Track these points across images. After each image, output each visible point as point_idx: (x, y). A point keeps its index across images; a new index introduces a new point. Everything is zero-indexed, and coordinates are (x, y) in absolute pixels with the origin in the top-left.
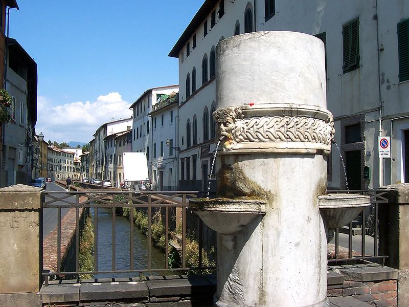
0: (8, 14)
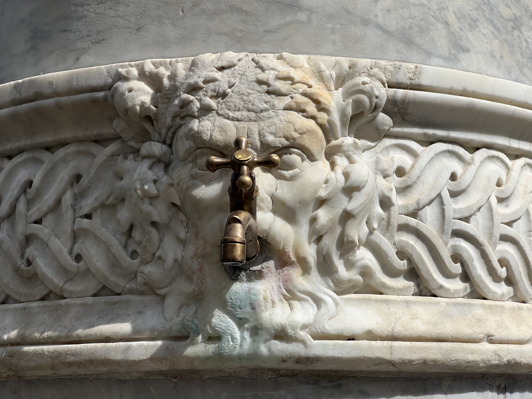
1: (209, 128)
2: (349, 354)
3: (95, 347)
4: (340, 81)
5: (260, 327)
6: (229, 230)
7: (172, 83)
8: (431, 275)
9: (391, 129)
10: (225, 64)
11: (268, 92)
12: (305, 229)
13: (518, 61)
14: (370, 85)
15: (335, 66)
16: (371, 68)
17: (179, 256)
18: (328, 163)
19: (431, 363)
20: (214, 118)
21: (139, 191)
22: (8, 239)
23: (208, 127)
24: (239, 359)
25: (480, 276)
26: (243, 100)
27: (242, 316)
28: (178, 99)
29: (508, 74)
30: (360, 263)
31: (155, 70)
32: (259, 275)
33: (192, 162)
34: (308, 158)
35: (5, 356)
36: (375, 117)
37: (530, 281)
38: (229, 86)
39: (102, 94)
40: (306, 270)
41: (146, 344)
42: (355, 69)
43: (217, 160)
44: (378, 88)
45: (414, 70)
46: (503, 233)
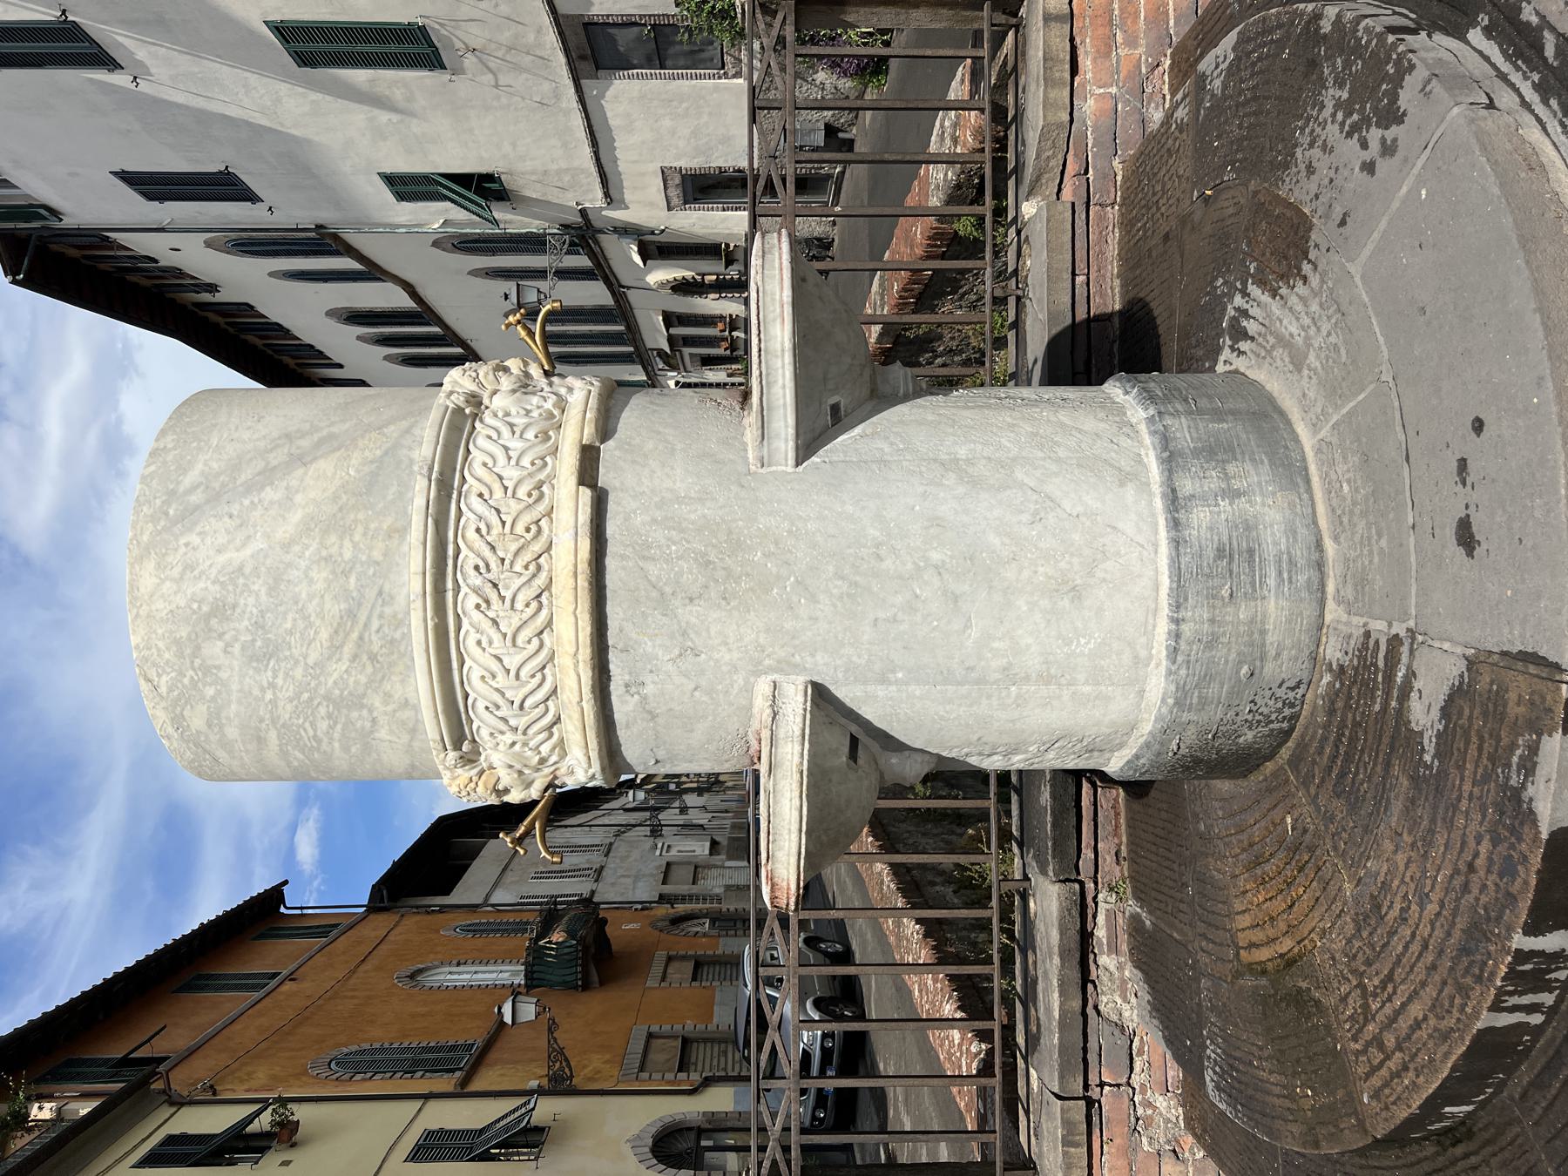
0: (302, 908)
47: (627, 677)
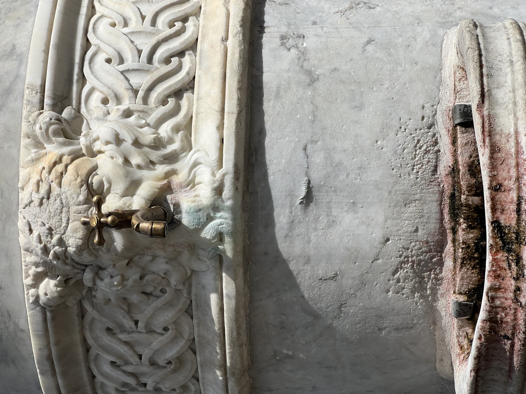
1: (74, 240)
2: (233, 143)
3: (227, 318)
4: (39, 145)
5: (213, 206)
6: (144, 232)
7: (41, 265)
8: (179, 81)
9: (74, 107)
10: (27, 228)
11: (48, 198)
12: (145, 173)
13: (21, 4)
14: (42, 124)
15: (28, 149)
16: (29, 122)
17: (165, 260)
18: (98, 155)
19: (240, 84)
20: (67, 237)
21: (119, 288)
22: (152, 377)
23: (73, 241)
24: (235, 220)
25: (180, 43)
26: (54, 216)
27: (205, 218)
28: (52, 261)
29: (32, 13)
30: (170, 134)
31: (31, 277)
32: (177, 206)
33: (98, 251)
34: (95, 170)
35: (234, 378)
36: (65, 120)
37: (185, 3)
38: (43, 226)
39: (48, 314)
40: (174, 172)
41: (225, 284)
42: (30, 134)
43: (96, 239)
44: (45, 118)
45: (30, 90)
46: (150, 23)
47: (284, 29)
